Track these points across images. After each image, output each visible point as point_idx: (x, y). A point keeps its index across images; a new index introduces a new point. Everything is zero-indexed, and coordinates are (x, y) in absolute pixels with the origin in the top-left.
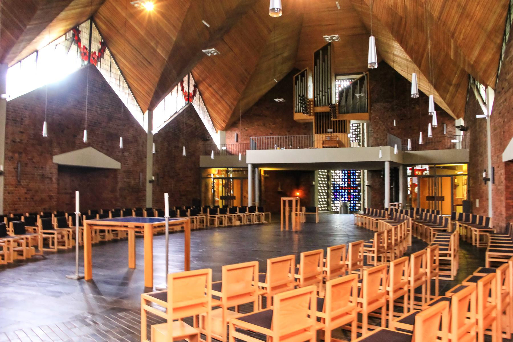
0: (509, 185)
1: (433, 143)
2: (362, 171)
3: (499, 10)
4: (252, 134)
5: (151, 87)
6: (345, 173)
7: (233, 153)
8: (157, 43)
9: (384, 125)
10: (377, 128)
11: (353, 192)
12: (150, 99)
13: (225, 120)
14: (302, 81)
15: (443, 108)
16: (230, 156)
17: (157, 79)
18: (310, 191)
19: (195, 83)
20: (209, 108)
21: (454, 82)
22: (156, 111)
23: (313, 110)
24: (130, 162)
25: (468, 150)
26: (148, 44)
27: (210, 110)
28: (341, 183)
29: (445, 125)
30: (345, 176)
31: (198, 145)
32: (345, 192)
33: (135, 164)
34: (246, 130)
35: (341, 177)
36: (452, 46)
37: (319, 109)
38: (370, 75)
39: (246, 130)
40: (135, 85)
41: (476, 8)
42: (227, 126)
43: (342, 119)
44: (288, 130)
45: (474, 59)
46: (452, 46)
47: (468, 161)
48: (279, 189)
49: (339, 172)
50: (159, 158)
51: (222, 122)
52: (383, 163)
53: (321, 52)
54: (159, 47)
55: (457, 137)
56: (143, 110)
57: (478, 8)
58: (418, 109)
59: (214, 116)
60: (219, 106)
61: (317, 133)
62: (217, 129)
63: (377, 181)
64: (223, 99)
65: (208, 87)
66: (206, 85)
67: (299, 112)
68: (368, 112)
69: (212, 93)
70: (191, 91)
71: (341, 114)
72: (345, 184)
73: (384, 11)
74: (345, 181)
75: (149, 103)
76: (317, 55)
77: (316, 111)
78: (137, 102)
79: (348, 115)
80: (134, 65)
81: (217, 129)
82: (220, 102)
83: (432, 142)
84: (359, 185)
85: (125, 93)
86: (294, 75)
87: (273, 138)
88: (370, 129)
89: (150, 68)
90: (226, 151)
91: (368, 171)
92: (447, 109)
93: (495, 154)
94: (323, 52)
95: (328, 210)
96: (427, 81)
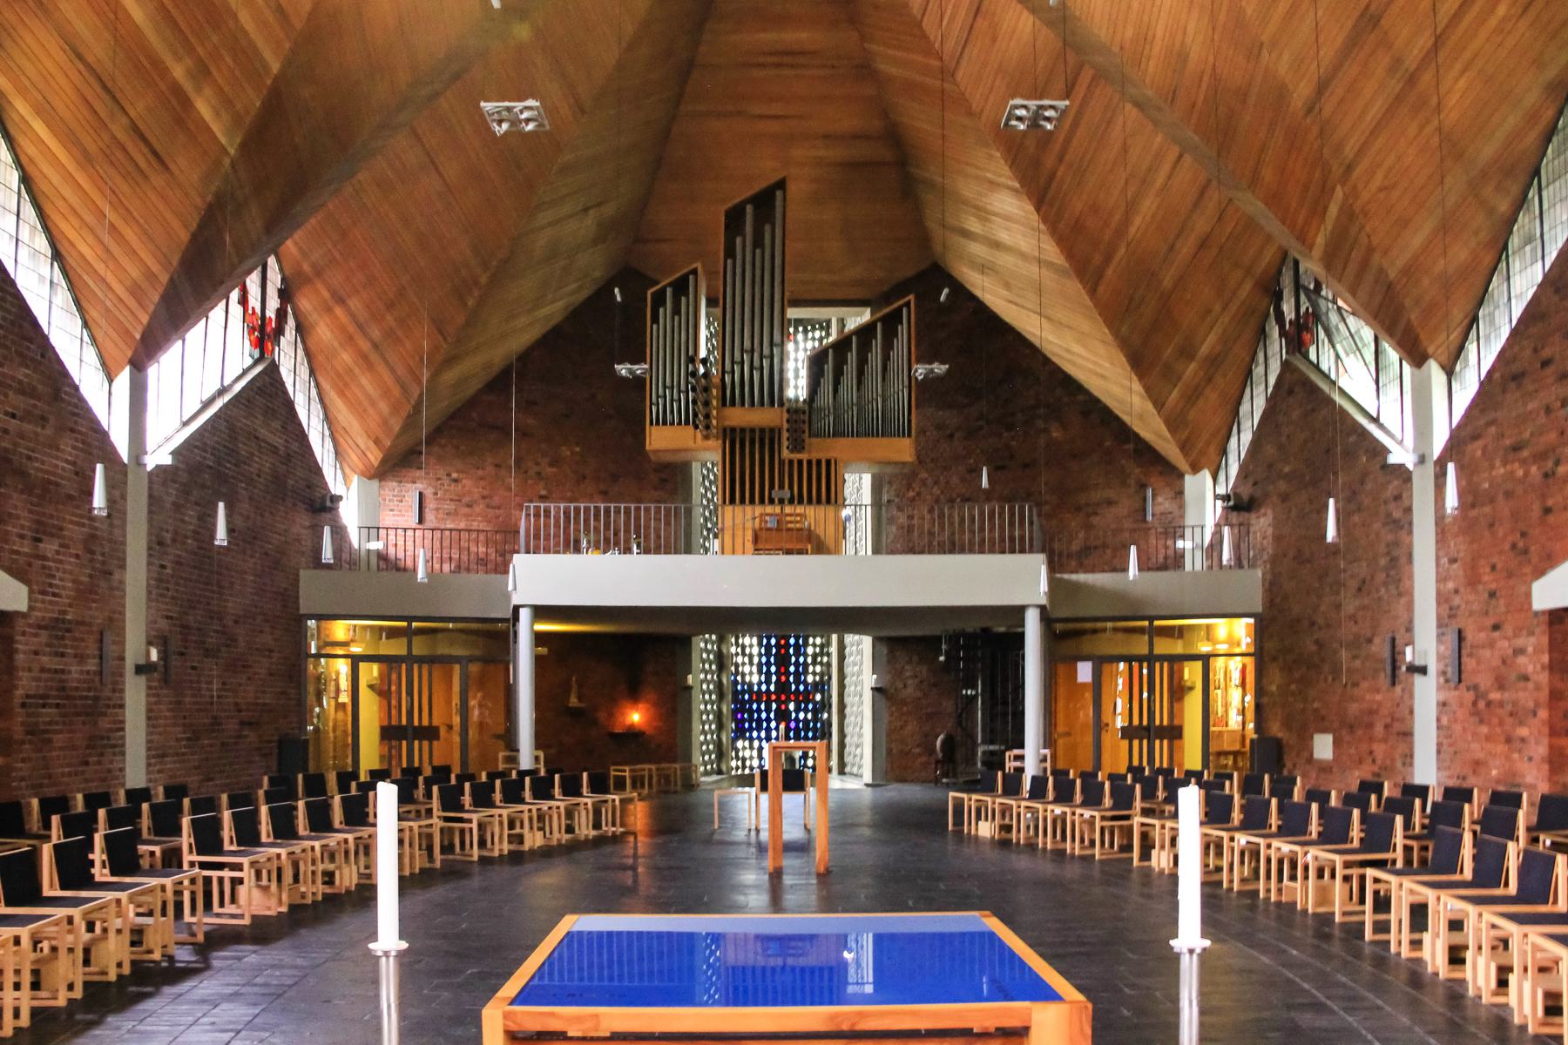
0: (1559, 685)
1: (1109, 551)
3: (1532, 97)
4: (476, 496)
5: (155, 268)
6: (768, 647)
7: (402, 564)
8: (202, 72)
9: (936, 483)
10: (911, 494)
11: (797, 710)
12: (145, 319)
13: (382, 436)
14: (676, 311)
15: (1145, 434)
16: (398, 574)
17: (184, 236)
18: (675, 703)
19: (283, 280)
20: (326, 386)
21: (1204, 350)
22: (164, 370)
23: (717, 418)
24: (66, 587)
25: (1259, 573)
26: (164, 72)
27: (332, 395)
28: (755, 679)
29: (1150, 492)
30: (768, 654)
31: (296, 529)
32: (768, 710)
33: (86, 593)
34: (456, 481)
35: (756, 660)
36: (1333, 210)
37: (740, 417)
38: (916, 305)
39: (456, 481)
40: (83, 246)
41: (1457, 80)
42: (383, 462)
43: (823, 456)
44: (602, 487)
45: (1400, 263)
46: (1333, 210)
47: (1259, 609)
48: (573, 701)
49: (866, 642)
50: (169, 571)
51: (371, 444)
52: (1018, 612)
53: (749, 209)
54: (208, 91)
55: (1188, 532)
56: (110, 363)
57: (1462, 83)
58: (1056, 434)
59: (340, 417)
60: (364, 381)
61: (732, 501)
62: (348, 471)
63: (908, 674)
64: (382, 356)
65: (331, 302)
66: (326, 294)
67: (665, 423)
69: (343, 329)
70: (271, 313)
71: (817, 436)
72: (768, 682)
73: (997, 83)
74: (768, 674)
75: (138, 336)
76: (734, 218)
77: (728, 423)
78: (86, 325)
79: (843, 441)
80: (85, 153)
81: (348, 471)
82: (370, 366)
83: (1105, 546)
84: (822, 686)
85: (41, 278)
86: (647, 289)
87: (547, 512)
89: (158, 180)
90: (382, 557)
91: (877, 641)
92: (1160, 436)
93: (1473, 581)
94: (756, 209)
95: (720, 772)
96: (1109, 338)
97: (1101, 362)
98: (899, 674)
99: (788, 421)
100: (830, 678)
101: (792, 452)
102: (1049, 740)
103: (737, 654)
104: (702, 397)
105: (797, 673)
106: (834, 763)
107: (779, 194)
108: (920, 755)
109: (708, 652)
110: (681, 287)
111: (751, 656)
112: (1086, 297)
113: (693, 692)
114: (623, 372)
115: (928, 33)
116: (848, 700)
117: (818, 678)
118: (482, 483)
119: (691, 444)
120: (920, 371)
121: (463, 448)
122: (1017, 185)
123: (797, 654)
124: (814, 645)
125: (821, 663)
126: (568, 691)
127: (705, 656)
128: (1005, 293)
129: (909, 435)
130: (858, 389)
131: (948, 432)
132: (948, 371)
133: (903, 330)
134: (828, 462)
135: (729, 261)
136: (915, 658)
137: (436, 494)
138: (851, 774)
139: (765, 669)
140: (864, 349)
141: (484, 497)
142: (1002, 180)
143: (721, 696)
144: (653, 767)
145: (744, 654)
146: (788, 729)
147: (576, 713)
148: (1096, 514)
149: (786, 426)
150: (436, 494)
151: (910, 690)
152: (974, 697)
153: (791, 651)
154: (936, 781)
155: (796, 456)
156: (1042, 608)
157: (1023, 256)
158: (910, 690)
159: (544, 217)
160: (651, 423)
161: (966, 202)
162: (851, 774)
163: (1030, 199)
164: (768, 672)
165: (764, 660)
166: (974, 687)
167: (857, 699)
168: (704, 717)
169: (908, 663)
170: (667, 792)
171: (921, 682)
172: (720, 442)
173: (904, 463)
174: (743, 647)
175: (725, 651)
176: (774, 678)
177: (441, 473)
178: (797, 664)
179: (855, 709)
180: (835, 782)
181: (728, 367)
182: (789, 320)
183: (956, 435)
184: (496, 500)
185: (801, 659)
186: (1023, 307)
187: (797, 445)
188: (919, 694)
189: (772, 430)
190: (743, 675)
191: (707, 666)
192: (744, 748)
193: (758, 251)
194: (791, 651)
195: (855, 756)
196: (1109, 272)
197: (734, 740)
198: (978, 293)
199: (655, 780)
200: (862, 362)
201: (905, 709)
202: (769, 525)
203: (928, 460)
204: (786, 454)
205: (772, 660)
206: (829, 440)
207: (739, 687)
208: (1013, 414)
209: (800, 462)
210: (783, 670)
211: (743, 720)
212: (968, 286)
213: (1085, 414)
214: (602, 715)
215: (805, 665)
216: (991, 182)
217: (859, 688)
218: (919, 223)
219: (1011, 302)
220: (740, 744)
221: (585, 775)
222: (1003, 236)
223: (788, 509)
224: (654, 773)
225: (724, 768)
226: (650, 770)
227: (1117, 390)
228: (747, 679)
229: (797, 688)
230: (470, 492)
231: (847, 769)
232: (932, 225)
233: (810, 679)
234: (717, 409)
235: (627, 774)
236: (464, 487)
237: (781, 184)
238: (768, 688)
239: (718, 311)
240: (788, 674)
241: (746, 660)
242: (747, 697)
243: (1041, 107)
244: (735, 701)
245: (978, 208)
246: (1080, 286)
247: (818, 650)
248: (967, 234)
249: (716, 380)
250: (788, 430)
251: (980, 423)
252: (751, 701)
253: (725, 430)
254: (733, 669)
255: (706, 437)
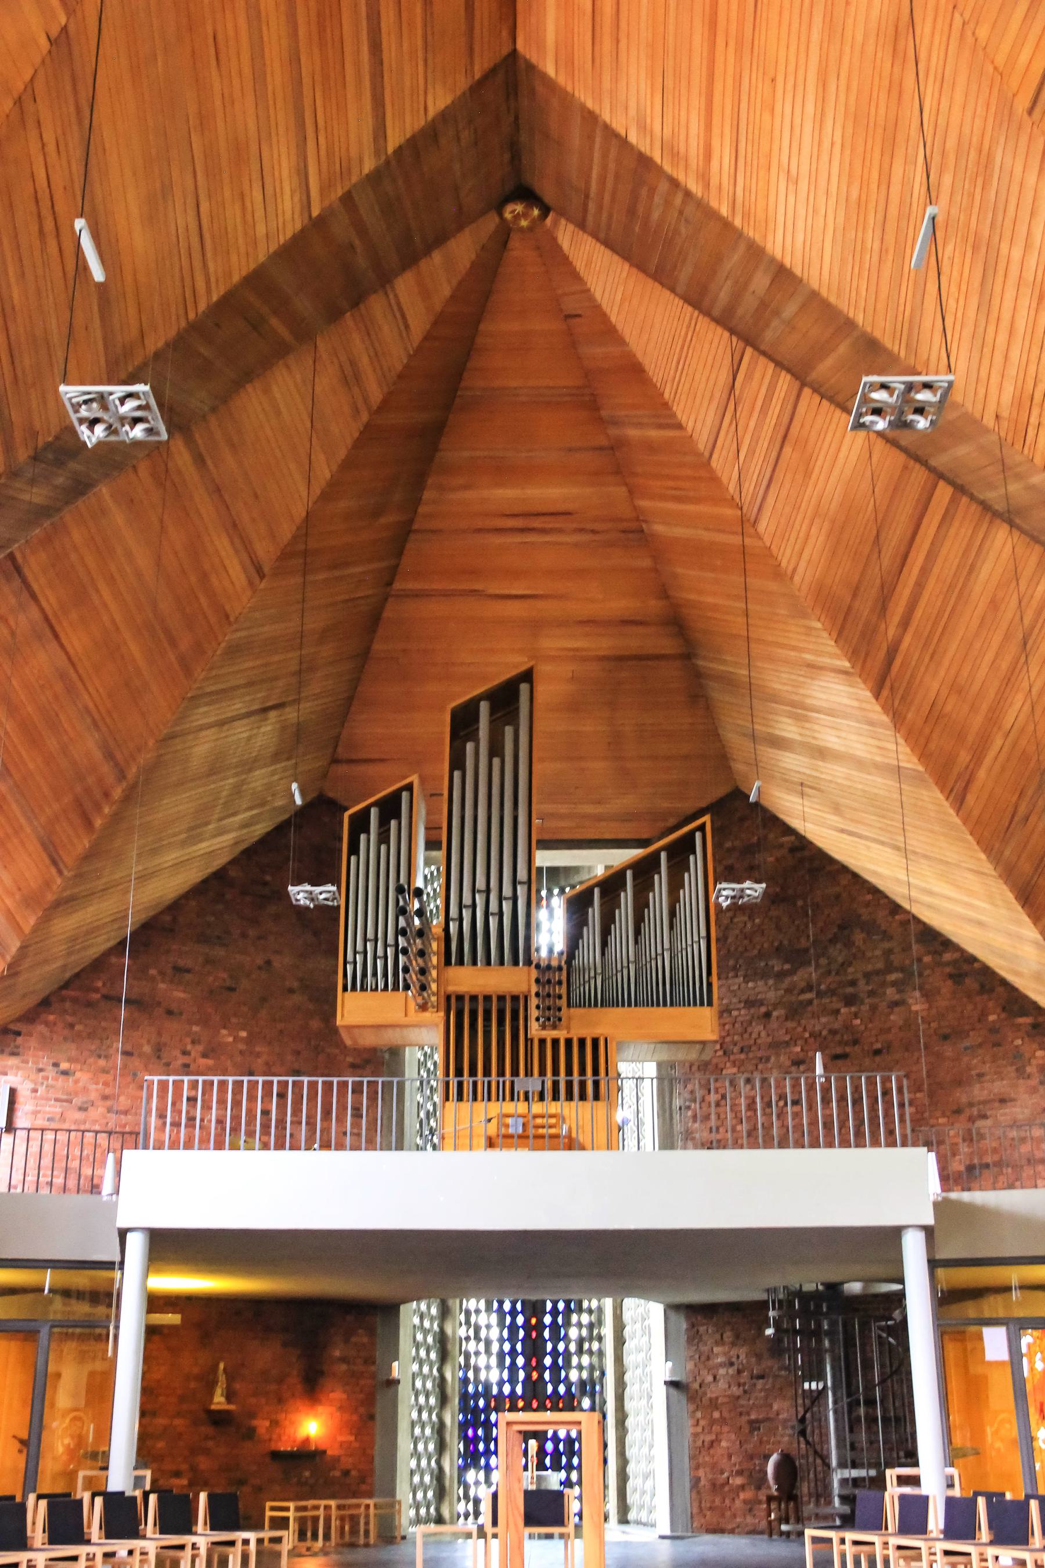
2: (608, 1303)
4: (93, 1096)
14: (384, 838)
23: (438, 981)
28: (494, 1376)
30: (513, 1338)
34: (65, 1073)
35: (495, 1347)
39: (65, 1073)
43: (588, 1033)
48: (219, 1401)
53: (484, 707)
67: (363, 989)
68: (710, 1004)
77: (451, 989)
84: (590, 1387)
88: (677, 1102)
91: (672, 1308)
96: (988, 868)
97: (977, 903)
98: (704, 1359)
99: (537, 981)
100: (603, 1374)
101: (544, 1027)
102: (952, 1454)
103: (468, 1339)
104: (416, 964)
105: (555, 1368)
106: (612, 1506)
107: (524, 687)
108: (742, 1487)
109: (426, 1332)
110: (390, 808)
111: (488, 1343)
112: (952, 812)
113: (400, 1387)
114: (300, 896)
115: (719, 473)
116: (629, 1406)
117: (585, 1375)
118: (103, 1078)
119: (398, 1016)
120: (725, 893)
121: (78, 1027)
122: (847, 664)
123: (556, 1338)
124: (580, 1325)
125: (590, 1352)
126: (210, 1387)
127: (420, 1337)
128: (834, 819)
129: (710, 1004)
130: (636, 942)
131: (763, 1009)
132: (765, 893)
133: (696, 862)
134: (595, 1042)
135: (457, 774)
136: (728, 1335)
137: (35, 1091)
138: (638, 1523)
139: (508, 1360)
140: (644, 887)
141: (105, 1098)
142: (827, 661)
143: (443, 1400)
144: (333, 1503)
145: (477, 1338)
146: (541, 1452)
147: (219, 1420)
148: (984, 1117)
149: (534, 989)
150: (35, 1091)
151: (722, 1384)
152: (822, 1393)
153: (546, 1334)
154: (771, 1531)
155: (550, 1034)
156: (929, 1232)
157: (860, 764)
158: (722, 1384)
159: (204, 715)
160: (345, 989)
161: (774, 698)
162: (638, 1523)
163: (865, 682)
164: (513, 1366)
165: (507, 1347)
166: (820, 1376)
167: (644, 1402)
168: (417, 1431)
169: (717, 1344)
170: (353, 1545)
171: (739, 1372)
172: (442, 1014)
173: (704, 1043)
174: (477, 1329)
175: (449, 1330)
176: (522, 1375)
177: (45, 1061)
178: (555, 1353)
179: (641, 1418)
180: (613, 1531)
181: (454, 912)
182: (540, 870)
183: (775, 1014)
184: (124, 1102)
185: (561, 1347)
186: (860, 836)
187: (551, 1018)
188: (736, 1390)
189: (515, 998)
190: (477, 1370)
191: (423, 1353)
192: (477, 1483)
193: (496, 761)
194: (546, 1334)
195: (644, 1493)
196: (982, 774)
197: (463, 1470)
198: (796, 823)
199: (334, 1524)
200: (641, 906)
201: (716, 1415)
202: (511, 1131)
203: (736, 1049)
204: (535, 1030)
205: (519, 1347)
206: (593, 1010)
207: (471, 1389)
208: (853, 983)
209: (555, 1042)
210: (534, 1363)
211: (476, 1439)
212: (782, 816)
213: (957, 978)
214: (262, 1425)
215: (567, 1354)
216: (811, 666)
217: (646, 1385)
218: (713, 734)
219: (842, 831)
220: (471, 1476)
221: (203, 1497)
222: (830, 739)
223: (537, 1108)
224: (334, 1513)
225: (446, 1513)
226: (327, 1508)
227: (1000, 941)
228: (483, 1376)
229: (555, 1390)
230: (85, 1089)
231: (631, 1516)
232: (732, 738)
233: (574, 1376)
234: (437, 968)
235: (291, 1514)
236: (76, 1082)
237: (527, 676)
238: (513, 1391)
239: (440, 855)
240: (541, 1368)
241: (482, 1347)
242: (481, 1403)
243: (910, 387)
244: (464, 1408)
245: (793, 704)
246: (941, 796)
247: (584, 1332)
248: (778, 743)
249: (437, 923)
250: (537, 995)
251: (808, 996)
252: (487, 1409)
253: (448, 998)
254: (462, 1359)
255: (423, 1007)
